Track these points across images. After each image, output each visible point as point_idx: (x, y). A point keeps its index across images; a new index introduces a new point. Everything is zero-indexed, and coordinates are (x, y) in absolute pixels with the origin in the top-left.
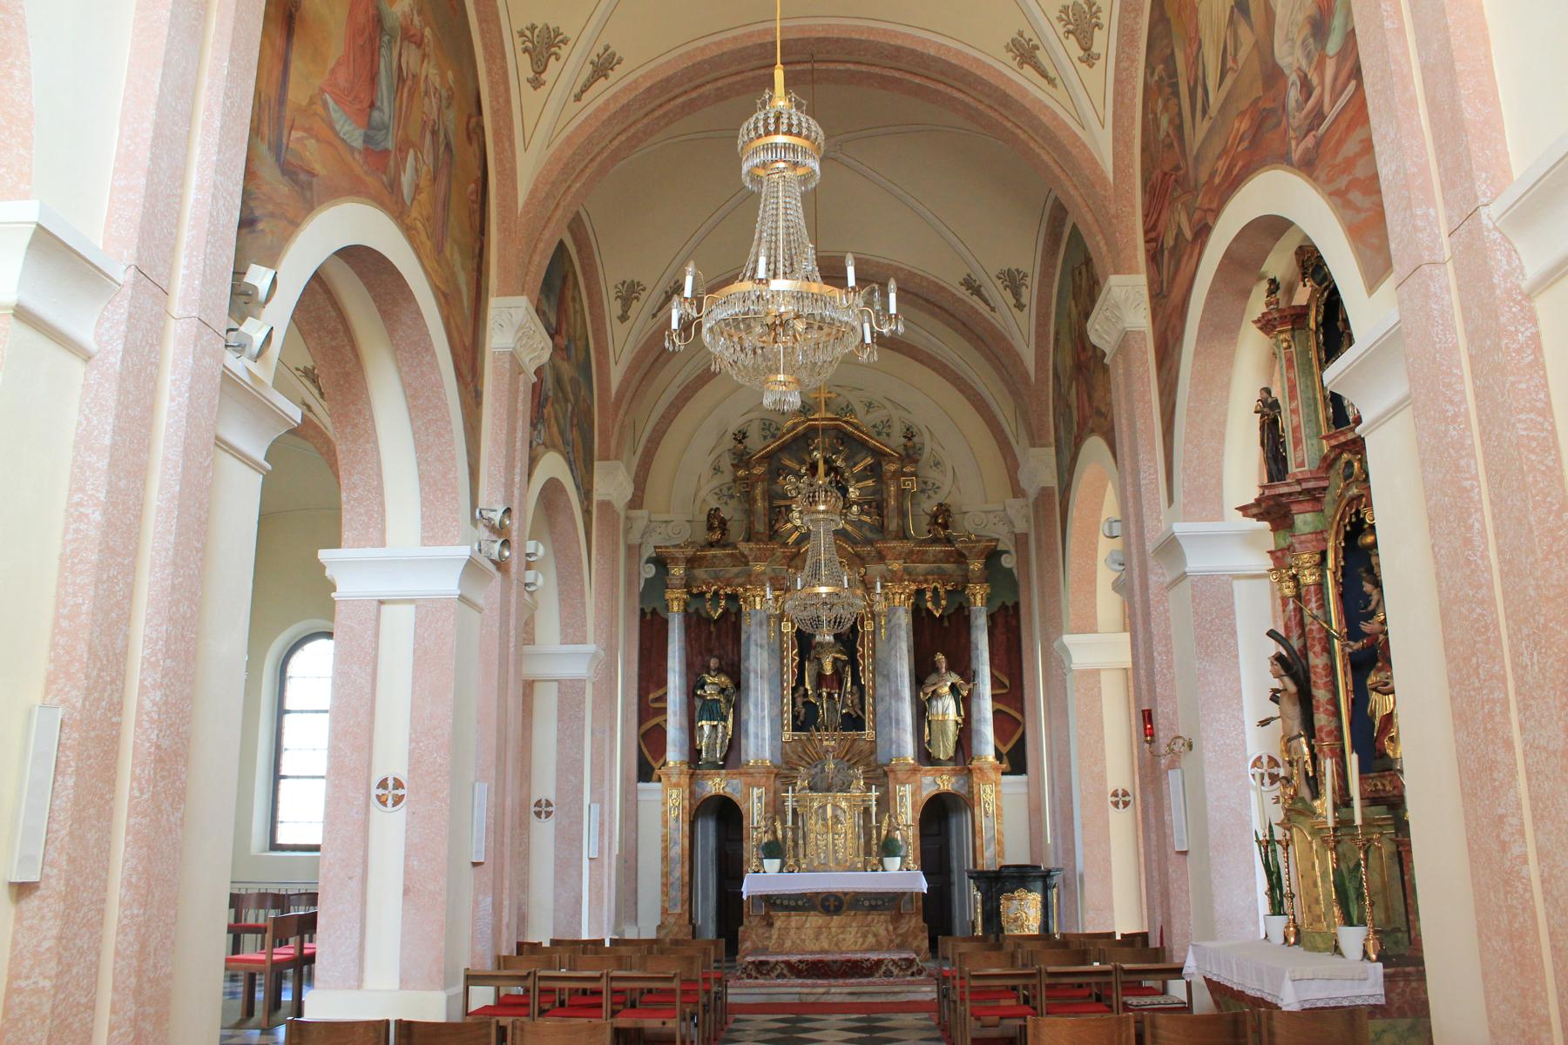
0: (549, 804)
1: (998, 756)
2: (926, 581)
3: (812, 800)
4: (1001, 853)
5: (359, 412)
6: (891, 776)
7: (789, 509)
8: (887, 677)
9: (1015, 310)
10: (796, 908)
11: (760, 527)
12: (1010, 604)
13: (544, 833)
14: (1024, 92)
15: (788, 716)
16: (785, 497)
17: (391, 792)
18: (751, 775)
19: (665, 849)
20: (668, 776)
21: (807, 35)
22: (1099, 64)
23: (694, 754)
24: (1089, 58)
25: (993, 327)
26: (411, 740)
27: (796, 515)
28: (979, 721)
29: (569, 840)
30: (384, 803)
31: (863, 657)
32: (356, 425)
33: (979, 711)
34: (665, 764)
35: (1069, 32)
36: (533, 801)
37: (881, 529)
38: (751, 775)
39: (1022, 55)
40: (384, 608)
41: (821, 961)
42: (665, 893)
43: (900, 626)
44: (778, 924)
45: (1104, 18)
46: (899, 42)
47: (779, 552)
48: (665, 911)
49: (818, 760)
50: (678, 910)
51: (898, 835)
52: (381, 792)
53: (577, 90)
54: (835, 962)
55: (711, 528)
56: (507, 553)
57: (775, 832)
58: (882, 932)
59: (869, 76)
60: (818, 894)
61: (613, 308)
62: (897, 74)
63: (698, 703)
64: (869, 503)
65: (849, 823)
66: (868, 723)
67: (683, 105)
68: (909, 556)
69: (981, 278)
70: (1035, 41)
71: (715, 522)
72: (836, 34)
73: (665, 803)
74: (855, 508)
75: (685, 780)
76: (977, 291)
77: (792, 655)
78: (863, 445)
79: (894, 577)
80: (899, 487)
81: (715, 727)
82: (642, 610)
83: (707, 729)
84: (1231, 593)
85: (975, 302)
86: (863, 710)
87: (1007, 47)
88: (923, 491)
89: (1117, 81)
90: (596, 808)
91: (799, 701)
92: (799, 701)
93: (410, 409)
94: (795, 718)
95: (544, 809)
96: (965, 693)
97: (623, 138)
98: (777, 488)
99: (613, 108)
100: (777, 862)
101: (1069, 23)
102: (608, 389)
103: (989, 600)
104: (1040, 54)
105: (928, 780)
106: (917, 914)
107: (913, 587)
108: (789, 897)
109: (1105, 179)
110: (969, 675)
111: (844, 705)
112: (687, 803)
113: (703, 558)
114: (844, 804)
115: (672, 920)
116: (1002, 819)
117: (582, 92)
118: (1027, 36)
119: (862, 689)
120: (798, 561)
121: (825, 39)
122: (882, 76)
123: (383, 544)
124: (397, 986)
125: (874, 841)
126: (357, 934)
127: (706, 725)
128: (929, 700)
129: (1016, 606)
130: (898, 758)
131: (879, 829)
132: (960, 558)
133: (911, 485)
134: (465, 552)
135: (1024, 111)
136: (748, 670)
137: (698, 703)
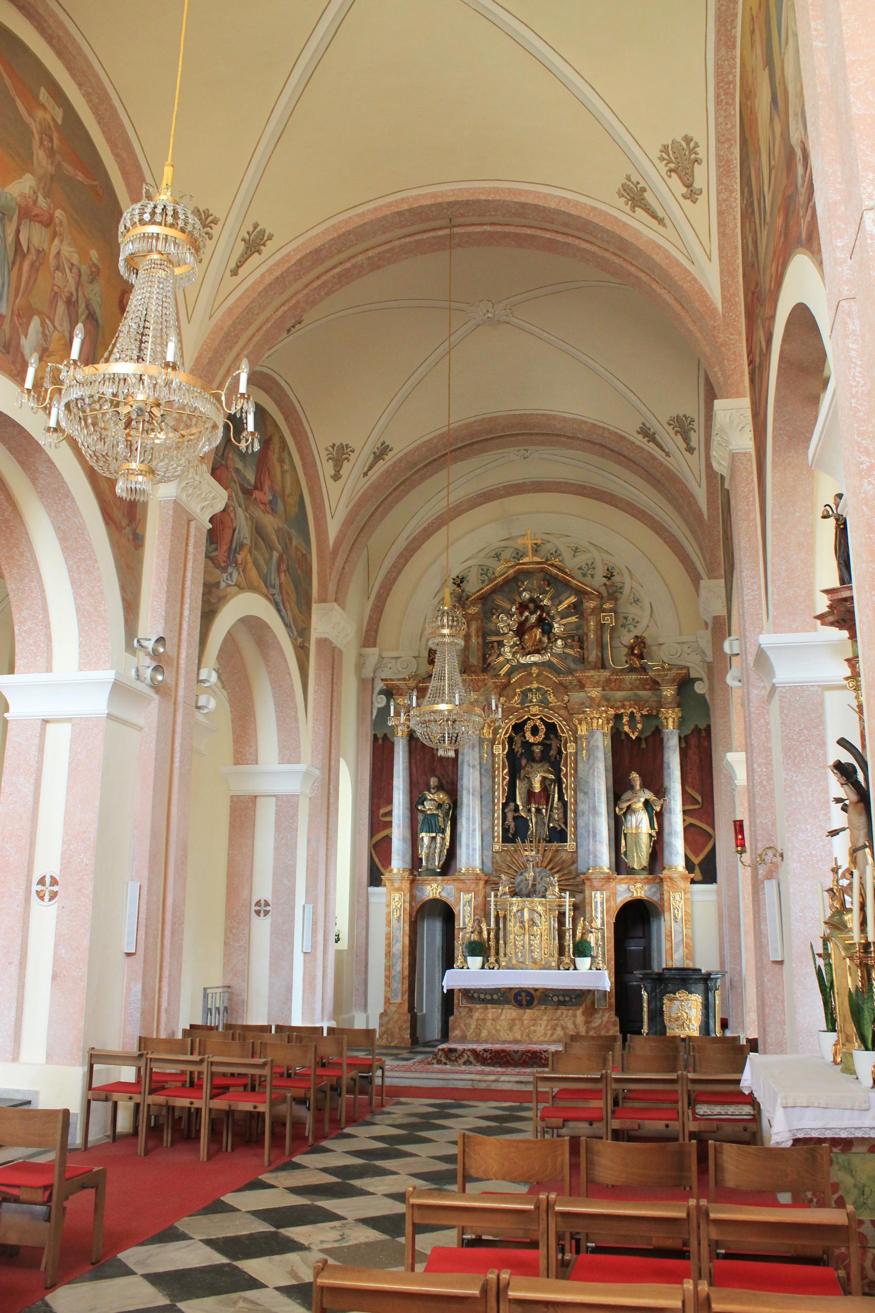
0: (267, 904)
2: (623, 707)
3: (511, 904)
4: (690, 955)
5: (22, 555)
6: (588, 883)
7: (501, 644)
9: (686, 454)
10: (492, 1002)
11: (474, 661)
12: (702, 726)
13: (262, 929)
14: (638, 234)
15: (498, 830)
16: (497, 633)
17: (49, 889)
18: (462, 881)
19: (389, 945)
21: (439, 200)
22: (702, 198)
23: (416, 862)
24: (692, 195)
25: (668, 470)
26: (64, 842)
27: (507, 649)
28: (670, 834)
29: (283, 936)
30: (42, 898)
31: (566, 775)
32: (20, 566)
33: (670, 824)
34: (391, 871)
35: (671, 171)
36: (254, 902)
37: (582, 660)
38: (462, 881)
39: (632, 199)
40: (49, 727)
41: (503, 1051)
42: (388, 985)
43: (597, 747)
44: (476, 1015)
45: (701, 152)
46: (523, 199)
47: (490, 682)
48: (387, 1001)
50: (399, 1000)
52: (40, 888)
53: (232, 265)
54: (516, 1052)
56: (160, 678)
57: (480, 933)
59: (506, 235)
60: (511, 989)
61: (326, 469)
62: (529, 231)
64: (572, 637)
65: (546, 925)
66: (570, 836)
67: (339, 275)
68: (606, 684)
69: (655, 426)
70: (642, 184)
72: (465, 197)
73: (390, 903)
74: (559, 642)
75: (406, 885)
76: (652, 438)
77: (502, 775)
78: (567, 585)
79: (593, 703)
81: (434, 838)
82: (375, 736)
83: (426, 841)
84: (822, 704)
85: (651, 448)
86: (566, 823)
87: (619, 193)
88: (623, 626)
89: (720, 213)
90: (309, 908)
91: (510, 816)
92: (510, 816)
93: (64, 549)
94: (505, 830)
95: (263, 908)
96: (658, 809)
97: (285, 308)
98: (491, 626)
99: (268, 280)
100: (479, 960)
101: (670, 162)
102: (327, 540)
103: (681, 723)
104: (648, 195)
105: (621, 888)
107: (612, 712)
108: (485, 991)
109: (715, 310)
110: (661, 792)
112: (407, 905)
114: (540, 909)
115: (393, 1008)
116: (690, 922)
117: (238, 267)
118: (634, 180)
119: (565, 804)
120: (509, 691)
121: (457, 203)
122: (517, 235)
123: (49, 669)
124: (44, 1061)
126: (13, 1014)
127: (425, 837)
128: (625, 814)
129: (708, 729)
130: (594, 868)
131: (574, 931)
132: (655, 685)
133: (608, 620)
134: (109, 675)
135: (640, 253)
136: (462, 786)
137: (420, 817)
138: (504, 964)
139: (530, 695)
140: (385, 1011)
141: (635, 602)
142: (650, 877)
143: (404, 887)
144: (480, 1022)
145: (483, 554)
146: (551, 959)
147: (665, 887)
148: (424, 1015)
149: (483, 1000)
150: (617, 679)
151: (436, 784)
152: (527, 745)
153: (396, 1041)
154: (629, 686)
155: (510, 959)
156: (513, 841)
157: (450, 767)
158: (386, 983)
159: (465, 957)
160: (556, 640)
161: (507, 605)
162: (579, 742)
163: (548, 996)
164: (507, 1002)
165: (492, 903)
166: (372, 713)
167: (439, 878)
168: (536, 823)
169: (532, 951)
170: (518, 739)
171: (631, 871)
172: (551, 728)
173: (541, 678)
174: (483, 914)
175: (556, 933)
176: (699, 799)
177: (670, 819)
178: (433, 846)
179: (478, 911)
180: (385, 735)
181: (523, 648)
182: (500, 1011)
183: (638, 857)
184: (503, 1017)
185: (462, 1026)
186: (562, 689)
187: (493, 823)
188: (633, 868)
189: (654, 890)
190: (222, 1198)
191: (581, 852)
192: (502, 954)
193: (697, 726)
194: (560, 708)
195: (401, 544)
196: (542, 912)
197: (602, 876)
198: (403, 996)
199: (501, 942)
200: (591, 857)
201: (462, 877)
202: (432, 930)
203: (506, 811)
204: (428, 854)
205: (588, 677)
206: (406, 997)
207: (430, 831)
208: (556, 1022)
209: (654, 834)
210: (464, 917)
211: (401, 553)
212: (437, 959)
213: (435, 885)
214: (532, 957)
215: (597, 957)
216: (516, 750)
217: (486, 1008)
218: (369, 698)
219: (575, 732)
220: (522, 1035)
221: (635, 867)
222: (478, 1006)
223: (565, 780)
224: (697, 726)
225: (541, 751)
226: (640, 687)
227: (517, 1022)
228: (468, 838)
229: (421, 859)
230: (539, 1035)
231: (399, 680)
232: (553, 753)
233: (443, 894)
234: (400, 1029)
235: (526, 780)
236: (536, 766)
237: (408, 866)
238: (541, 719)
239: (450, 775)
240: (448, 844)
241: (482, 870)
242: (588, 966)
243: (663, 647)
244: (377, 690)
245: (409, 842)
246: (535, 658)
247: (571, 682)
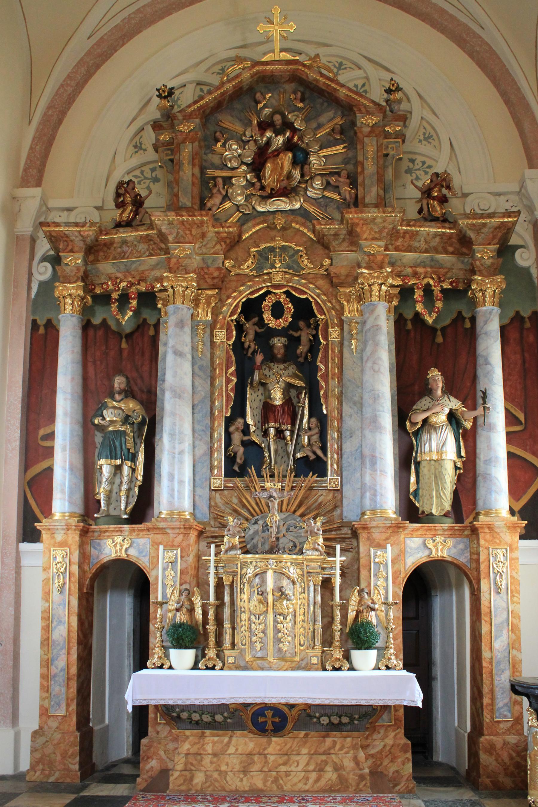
1: (512, 512)
2: (415, 275)
3: (244, 565)
6: (363, 536)
8: (360, 405)
10: (213, 725)
15: (220, 457)
18: (162, 531)
19: (47, 629)
20: (52, 531)
28: (488, 462)
31: (325, 377)
33: (489, 447)
38: (162, 531)
42: (45, 688)
47: (211, 231)
48: (44, 713)
49: (256, 512)
50: (62, 712)
51: (372, 617)
55: (120, 205)
57: (191, 611)
58: (348, 763)
60: (246, 705)
63: (99, 438)
65: (302, 599)
66: (331, 466)
71: (129, 199)
74: (318, 183)
75: (74, 538)
77: (227, 378)
80: (379, 147)
82: (34, 322)
88: (409, 171)
92: (237, 437)
94: (230, 460)
100: (189, 655)
106: (396, 725)
108: (202, 709)
111: (298, 446)
112: (75, 568)
113: (109, 245)
114: (293, 572)
115: (54, 724)
120: (239, 251)
125: (337, 627)
127: (105, 467)
128: (417, 434)
131: (344, 609)
132: (463, 244)
137: (99, 438)
138: (231, 660)
139: (271, 257)
140: (41, 728)
141: (426, 139)
142: (457, 526)
143: (70, 541)
144: (191, 759)
145: (204, 67)
146: (310, 652)
147: (482, 542)
148: (106, 729)
149: (197, 723)
150: (406, 232)
151: (123, 386)
152: (265, 335)
153: (57, 775)
154: (423, 246)
155: (242, 653)
156: (242, 472)
157: (146, 368)
158: (42, 685)
159: (166, 649)
160: (312, 178)
161: (238, 128)
162: (346, 327)
163: (310, 716)
164: (240, 726)
165: (212, 565)
166: (29, 288)
167: (126, 527)
168: (276, 451)
169: (279, 641)
170: (250, 328)
171: (429, 518)
172: (304, 310)
173: (289, 232)
174: (194, 583)
175: (319, 612)
176: (521, 417)
177: (489, 439)
178: (117, 481)
179: (188, 578)
180: (49, 321)
181: (263, 188)
182: (226, 740)
183: (439, 497)
184: (231, 750)
185: (162, 753)
186: (320, 250)
187: (211, 448)
188: (431, 514)
189: (461, 546)
191: (347, 491)
192: (227, 644)
193: (517, 313)
194: (316, 277)
195: (79, 46)
196: (295, 576)
197: (388, 523)
198: (68, 705)
199: (227, 625)
200: (368, 494)
201: (162, 525)
202: (117, 610)
203: (232, 429)
204: (111, 491)
205: (366, 222)
206: (74, 707)
207: (113, 456)
208: (324, 757)
210: (164, 586)
211: (82, 59)
212: (126, 648)
213: (119, 539)
214: (280, 650)
215: (386, 648)
216: (246, 345)
217: (203, 735)
218: (26, 264)
219: (341, 312)
220: (265, 781)
221: (434, 512)
222: (188, 733)
223: (323, 384)
224: (517, 313)
225: (286, 347)
226: (440, 249)
227: (256, 758)
228: (172, 465)
229: (99, 501)
230: (296, 780)
231: (67, 224)
232: (302, 349)
233: (132, 552)
234: (64, 756)
235: (261, 389)
236: (277, 367)
237: (79, 509)
238: (288, 293)
239: (146, 375)
240: (140, 478)
241: (193, 514)
242: (373, 665)
243: (470, 198)
244: (38, 255)
245: (80, 474)
246: (282, 204)
247: (336, 235)
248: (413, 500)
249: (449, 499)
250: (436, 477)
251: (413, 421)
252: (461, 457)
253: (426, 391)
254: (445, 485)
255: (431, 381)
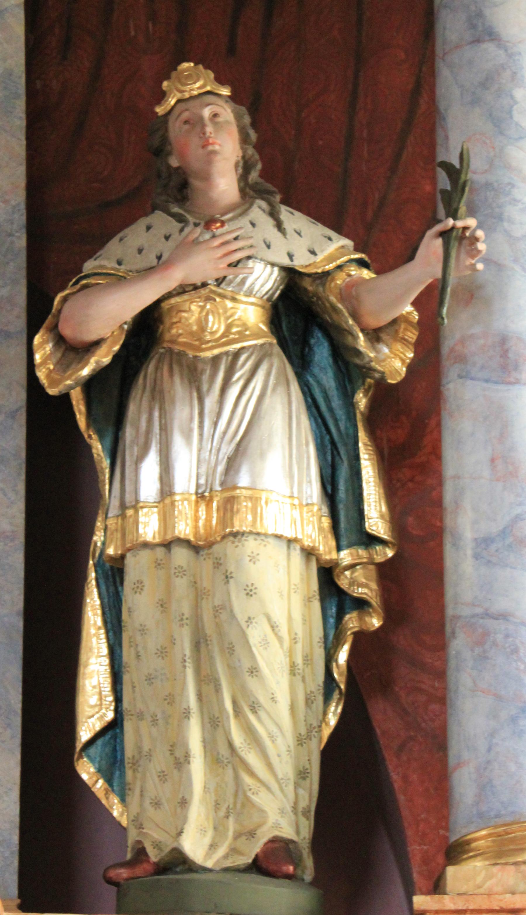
183: (224, 758)
190: (374, 276)
209: (362, 584)
221: (195, 845)
248: (99, 786)
249: (286, 768)
250: (199, 643)
251: (67, 331)
252: (371, 540)
253: (169, 187)
254: (252, 683)
255: (176, 129)
